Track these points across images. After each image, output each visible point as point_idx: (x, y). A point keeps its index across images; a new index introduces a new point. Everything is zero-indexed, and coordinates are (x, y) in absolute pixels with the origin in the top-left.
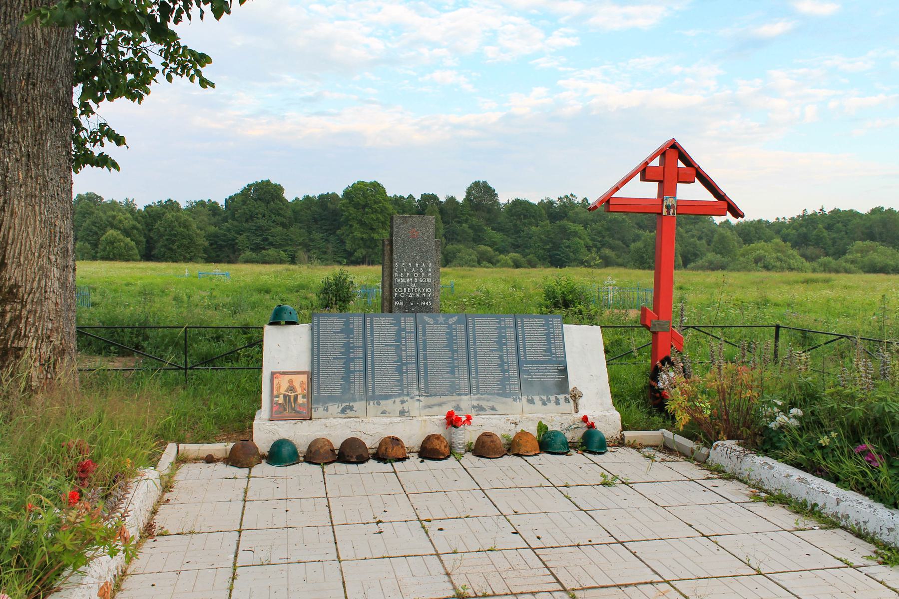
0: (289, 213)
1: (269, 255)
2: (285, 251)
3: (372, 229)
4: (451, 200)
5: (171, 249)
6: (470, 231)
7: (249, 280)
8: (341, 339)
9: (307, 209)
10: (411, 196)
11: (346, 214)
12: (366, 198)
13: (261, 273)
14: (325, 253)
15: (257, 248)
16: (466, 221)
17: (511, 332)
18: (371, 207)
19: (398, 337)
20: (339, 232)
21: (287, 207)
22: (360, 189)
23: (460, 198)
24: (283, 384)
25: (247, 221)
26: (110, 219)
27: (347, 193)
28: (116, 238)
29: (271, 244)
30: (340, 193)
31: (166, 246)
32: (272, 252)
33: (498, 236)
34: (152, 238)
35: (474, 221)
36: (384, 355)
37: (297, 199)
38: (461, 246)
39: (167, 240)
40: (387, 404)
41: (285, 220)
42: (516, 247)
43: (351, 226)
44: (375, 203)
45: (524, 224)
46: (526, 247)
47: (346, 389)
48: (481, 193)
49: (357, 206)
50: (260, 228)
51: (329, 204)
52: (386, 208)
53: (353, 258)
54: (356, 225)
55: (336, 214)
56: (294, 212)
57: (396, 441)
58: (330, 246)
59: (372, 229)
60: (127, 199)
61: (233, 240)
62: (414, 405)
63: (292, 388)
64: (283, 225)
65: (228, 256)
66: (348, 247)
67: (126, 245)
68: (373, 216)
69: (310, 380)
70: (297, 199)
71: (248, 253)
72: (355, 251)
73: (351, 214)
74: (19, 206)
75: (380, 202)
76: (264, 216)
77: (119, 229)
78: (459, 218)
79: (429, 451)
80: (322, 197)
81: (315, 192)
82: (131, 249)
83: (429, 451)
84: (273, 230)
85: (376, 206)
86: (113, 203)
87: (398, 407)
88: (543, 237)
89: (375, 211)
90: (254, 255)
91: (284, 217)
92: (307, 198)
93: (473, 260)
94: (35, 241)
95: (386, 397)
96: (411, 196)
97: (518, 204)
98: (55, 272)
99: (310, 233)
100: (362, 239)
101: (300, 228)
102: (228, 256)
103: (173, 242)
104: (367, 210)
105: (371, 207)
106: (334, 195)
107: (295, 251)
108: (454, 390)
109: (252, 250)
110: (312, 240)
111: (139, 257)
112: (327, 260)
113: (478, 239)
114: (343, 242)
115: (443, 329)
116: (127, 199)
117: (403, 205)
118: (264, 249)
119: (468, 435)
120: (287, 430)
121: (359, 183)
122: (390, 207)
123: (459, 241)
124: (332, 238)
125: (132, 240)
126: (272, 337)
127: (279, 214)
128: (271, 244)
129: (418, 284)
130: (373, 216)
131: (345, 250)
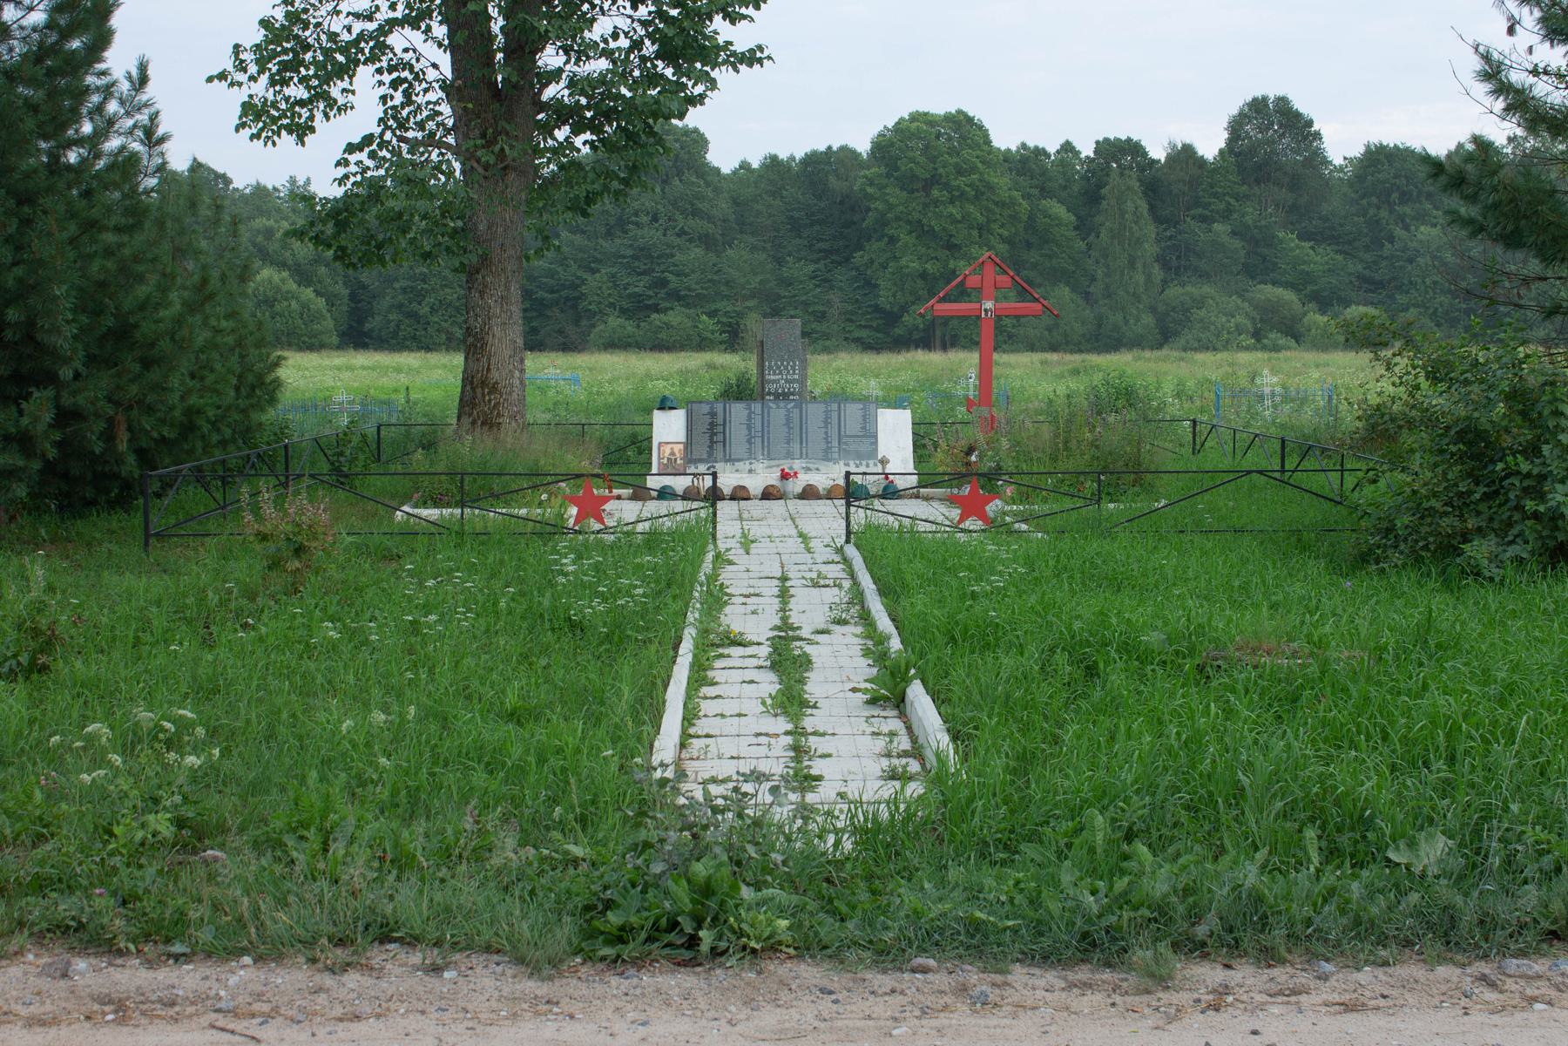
0: (723, 207)
1: (668, 326)
2: (711, 315)
3: (952, 247)
4: (1184, 155)
5: (414, 316)
6: (1237, 243)
7: (624, 388)
8: (708, 419)
9: (773, 194)
10: (1067, 147)
11: (879, 205)
12: (933, 160)
13: (648, 376)
14: (822, 317)
15: (639, 308)
16: (1226, 215)
17: (835, 415)
18: (946, 186)
19: (749, 418)
20: (859, 258)
21: (717, 190)
22: (916, 135)
23: (1210, 144)
24: (667, 450)
25: (609, 234)
26: (260, 239)
27: (882, 146)
28: (279, 290)
29: (676, 296)
30: (863, 146)
31: (400, 306)
32: (676, 317)
33: (1317, 258)
34: (364, 287)
35: (1250, 213)
36: (737, 433)
37: (745, 166)
38: (1206, 289)
39: (404, 290)
40: (740, 465)
41: (710, 229)
42: (1371, 286)
43: (893, 240)
44: (960, 172)
45: (1401, 219)
46: (1399, 288)
47: (710, 454)
48: (1272, 132)
49: (908, 183)
50: (643, 252)
51: (832, 179)
52: (990, 187)
53: (898, 331)
54: (905, 238)
55: (851, 206)
56: (735, 202)
57: (743, 488)
58: (835, 297)
59: (952, 247)
60: (293, 181)
61: (574, 287)
62: (759, 466)
63: (672, 453)
64: (707, 241)
65: (561, 332)
66: (884, 299)
67: (305, 306)
68: (954, 210)
69: (686, 448)
70: (745, 166)
71: (614, 321)
72: (904, 309)
73: (891, 207)
74: (497, 330)
75: (973, 169)
76: (655, 219)
77: (283, 265)
78: (1206, 206)
79: (768, 495)
80: (812, 159)
81: (794, 146)
82: (316, 317)
83: (768, 495)
84: (679, 257)
85: (960, 182)
86: (260, 191)
87: (748, 467)
88: (1448, 256)
89: (957, 197)
90: (630, 327)
91: (710, 219)
92: (773, 163)
93: (1239, 330)
94: (508, 352)
95: (739, 460)
96: (1067, 147)
97: (1379, 158)
98: (517, 374)
99: (780, 262)
100: (923, 275)
101: (754, 249)
102: (561, 332)
103: (420, 296)
104: (935, 193)
105: (946, 186)
106: (847, 153)
107: (740, 315)
108: (789, 455)
109: (623, 311)
110: (787, 283)
111: (335, 340)
112: (827, 337)
113: (1260, 267)
114: (870, 285)
115: (782, 412)
116: (293, 181)
117: (1044, 172)
118: (656, 309)
119: (796, 486)
120: (667, 481)
121: (916, 117)
122: (1002, 181)
123: (1204, 276)
124: (841, 276)
125: (318, 293)
126: (658, 416)
127: (696, 213)
128: (676, 296)
129: (787, 381)
130: (954, 210)
131: (877, 309)
